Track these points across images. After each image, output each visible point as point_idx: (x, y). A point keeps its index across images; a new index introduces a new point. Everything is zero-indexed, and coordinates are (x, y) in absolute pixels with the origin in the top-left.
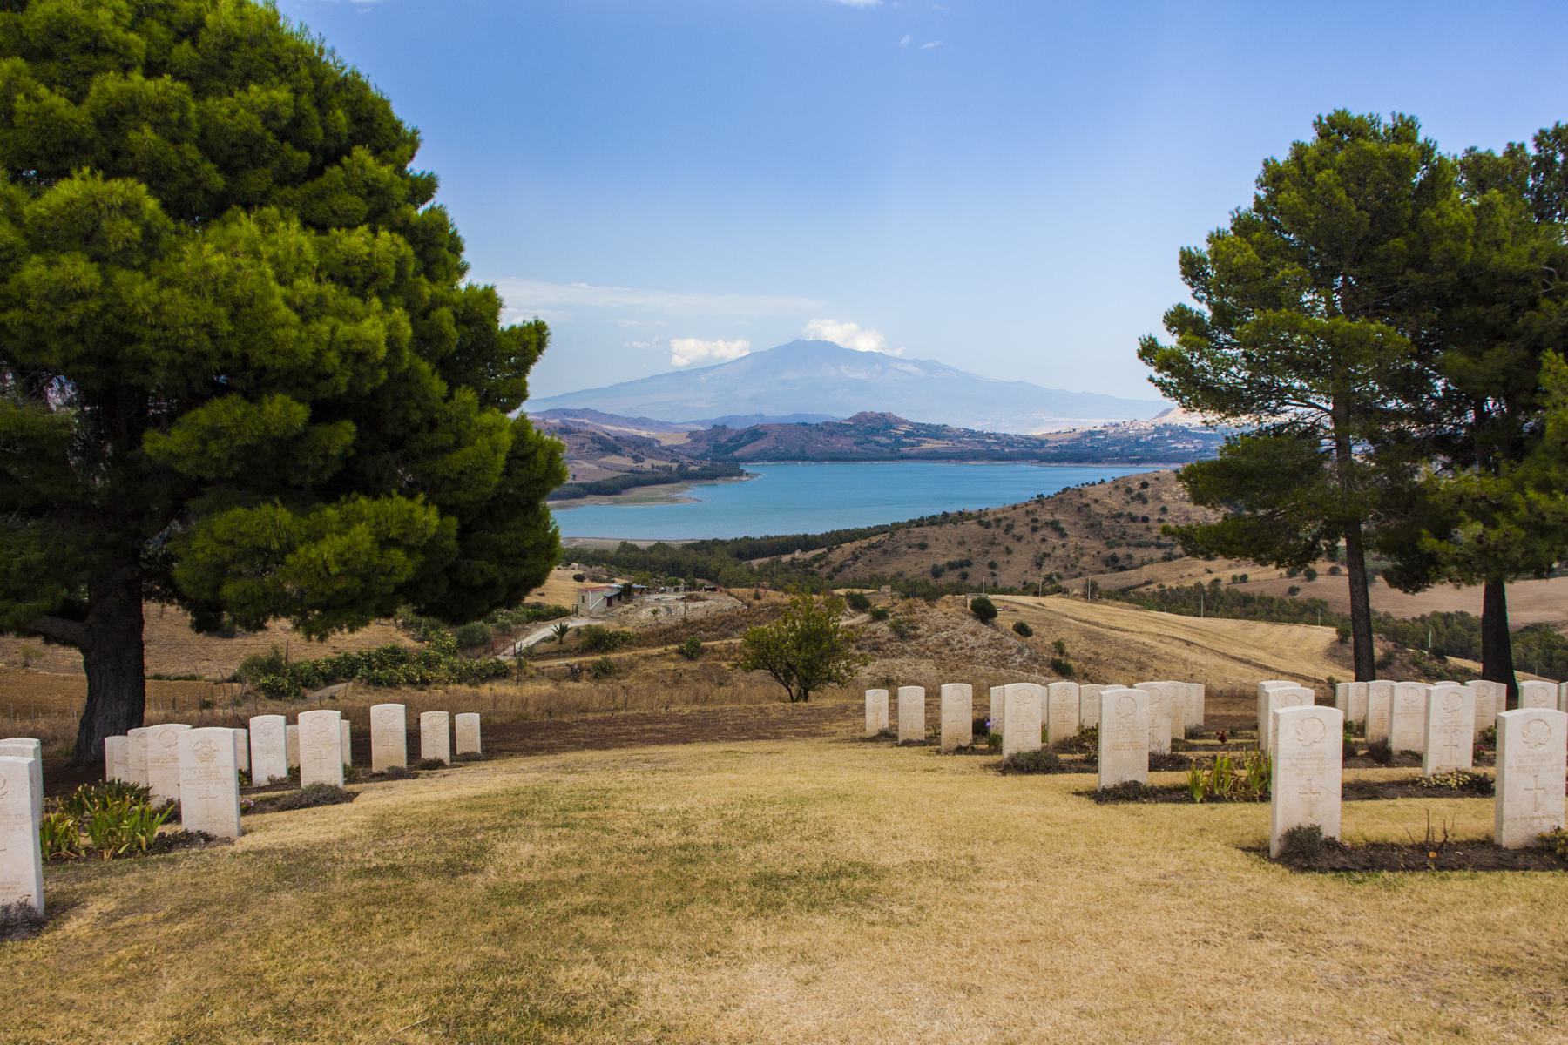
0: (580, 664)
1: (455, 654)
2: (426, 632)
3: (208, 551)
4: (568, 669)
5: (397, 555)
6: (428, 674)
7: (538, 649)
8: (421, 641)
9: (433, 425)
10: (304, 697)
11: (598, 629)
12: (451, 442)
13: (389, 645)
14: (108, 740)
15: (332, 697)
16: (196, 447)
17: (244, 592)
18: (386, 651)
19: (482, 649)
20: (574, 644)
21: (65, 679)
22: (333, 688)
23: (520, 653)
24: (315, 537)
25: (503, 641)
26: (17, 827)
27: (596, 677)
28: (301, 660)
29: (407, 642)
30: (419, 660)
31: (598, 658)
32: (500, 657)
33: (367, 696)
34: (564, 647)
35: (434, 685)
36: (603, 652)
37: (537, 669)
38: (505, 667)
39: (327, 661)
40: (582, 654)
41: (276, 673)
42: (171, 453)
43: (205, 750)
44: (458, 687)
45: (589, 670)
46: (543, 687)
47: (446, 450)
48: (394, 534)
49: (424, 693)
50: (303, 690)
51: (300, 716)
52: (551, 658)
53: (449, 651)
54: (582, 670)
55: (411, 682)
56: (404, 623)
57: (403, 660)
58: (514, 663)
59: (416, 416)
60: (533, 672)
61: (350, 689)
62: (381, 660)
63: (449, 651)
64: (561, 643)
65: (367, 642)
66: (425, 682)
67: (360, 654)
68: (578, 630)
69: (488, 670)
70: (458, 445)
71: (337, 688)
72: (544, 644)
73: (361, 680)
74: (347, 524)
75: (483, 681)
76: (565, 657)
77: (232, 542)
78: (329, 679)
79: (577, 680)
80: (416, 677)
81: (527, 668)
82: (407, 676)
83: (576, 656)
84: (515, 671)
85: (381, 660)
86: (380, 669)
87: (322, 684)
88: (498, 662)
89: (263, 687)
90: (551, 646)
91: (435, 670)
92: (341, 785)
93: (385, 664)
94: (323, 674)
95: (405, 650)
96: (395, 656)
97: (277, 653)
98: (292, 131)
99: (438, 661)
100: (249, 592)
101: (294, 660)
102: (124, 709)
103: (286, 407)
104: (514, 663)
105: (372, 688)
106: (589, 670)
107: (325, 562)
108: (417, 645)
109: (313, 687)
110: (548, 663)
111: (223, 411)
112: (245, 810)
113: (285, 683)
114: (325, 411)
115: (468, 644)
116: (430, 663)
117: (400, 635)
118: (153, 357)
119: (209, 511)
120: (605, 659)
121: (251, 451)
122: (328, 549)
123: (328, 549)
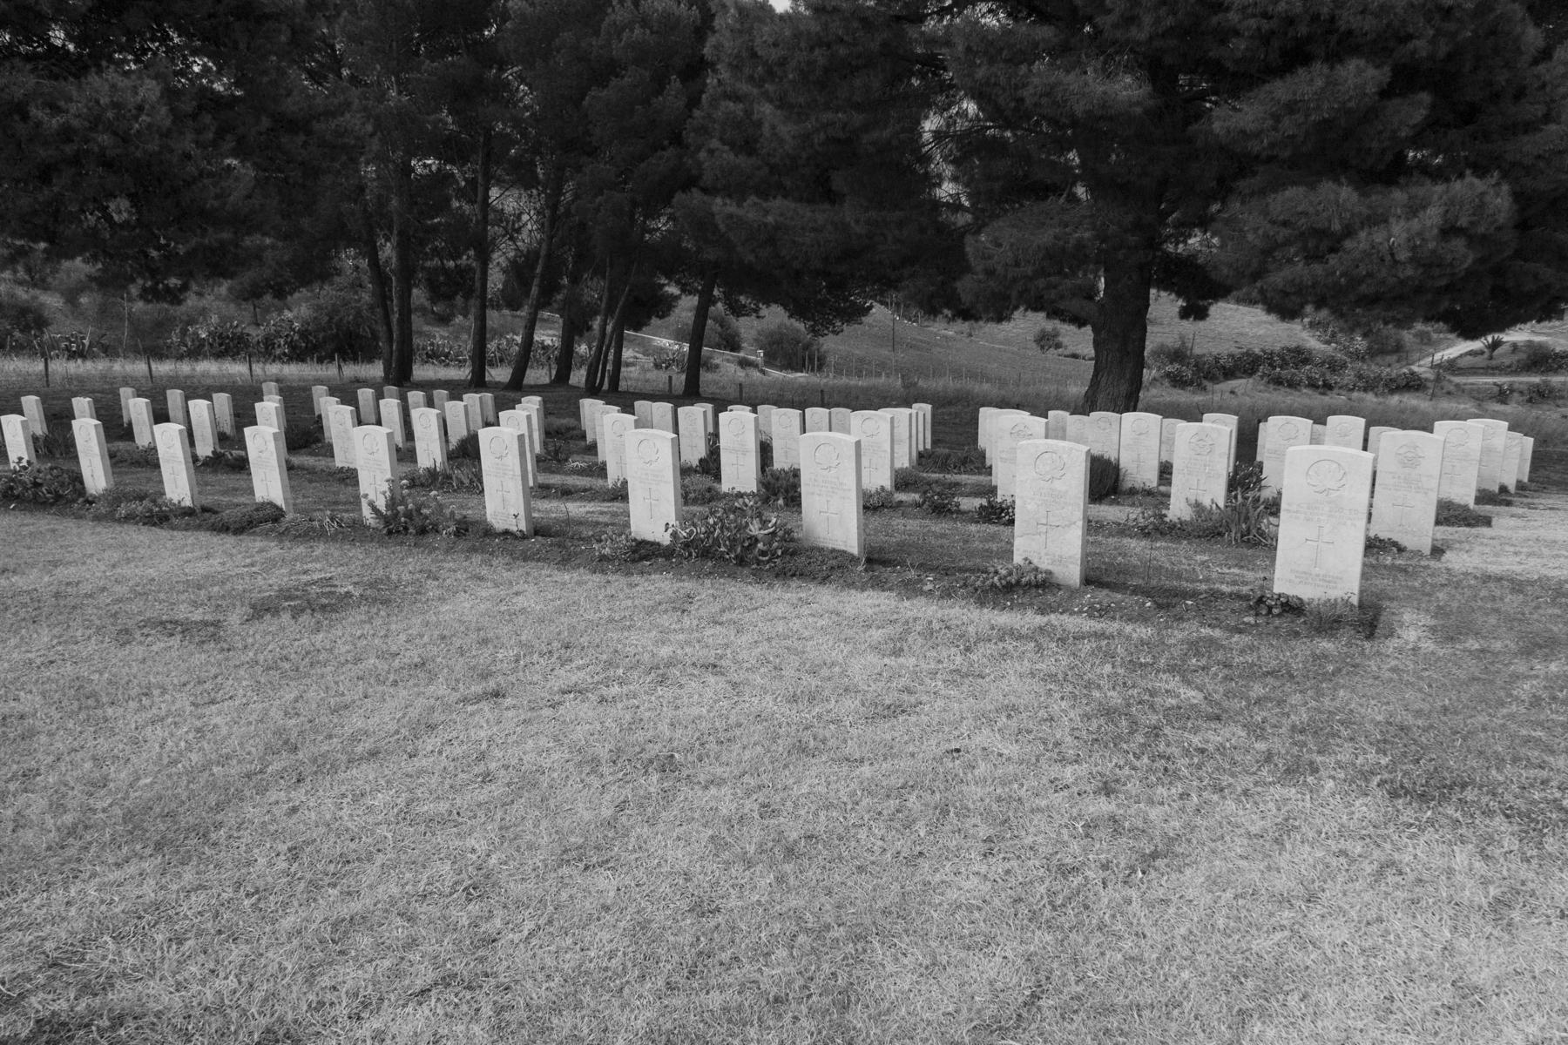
0: (1511, 384)
1: (1363, 359)
2: (1333, 335)
3: (1260, 232)
4: (1496, 389)
5: (1459, 244)
6: (1332, 379)
7: (1463, 363)
8: (1328, 343)
9: (1520, 94)
10: (1204, 389)
11: (1540, 345)
12: (1540, 114)
13: (1294, 345)
14: (982, 410)
15: (1232, 392)
16: (1270, 122)
17: (1293, 281)
18: (1289, 350)
19: (1395, 357)
20: (1507, 362)
21: (1000, 350)
22: (1233, 383)
23: (1439, 366)
24: (1377, 219)
25: (1420, 350)
26: (1349, 522)
27: (1530, 400)
28: (1205, 351)
29: (1312, 342)
30: (1323, 363)
31: (1536, 379)
32: (1415, 368)
33: (1267, 395)
34: (1494, 363)
35: (1336, 391)
36: (1543, 373)
37: (1457, 385)
38: (1419, 379)
39: (1229, 355)
40: (1516, 372)
41: (1182, 363)
42: (1243, 132)
43: (1409, 455)
44: (1362, 395)
45: (1521, 393)
46: (1462, 406)
47: (1529, 127)
48: (1463, 222)
49: (1326, 399)
50: (1205, 383)
51: (1437, 424)
52: (1475, 374)
53: (1358, 356)
54: (1512, 391)
55: (1313, 385)
56: (1311, 323)
57: (1306, 361)
58: (1430, 375)
59: (1502, 78)
60: (1452, 388)
61: (1250, 386)
62: (1283, 359)
63: (1358, 356)
64: (1491, 358)
65: (1269, 340)
66: (1328, 387)
67: (1263, 351)
68: (1515, 347)
69: (1399, 381)
70: (1547, 118)
71: (1239, 384)
72: (1469, 357)
73: (1262, 377)
74: (1414, 210)
75: (1392, 392)
76: (1493, 375)
77: (1285, 224)
78: (1229, 373)
79: (1504, 402)
80: (1318, 380)
81: (1445, 383)
82: (1309, 378)
83: (1507, 374)
84: (1430, 385)
85: (1283, 359)
86: (1281, 367)
87: (1221, 378)
88: (1413, 373)
89: (1168, 375)
90: (1480, 361)
91: (1340, 375)
92: (1472, 505)
93: (1287, 364)
94: (1224, 367)
95: (1310, 352)
96: (1300, 356)
97: (1183, 343)
99: (1344, 366)
100: (1297, 281)
101: (1197, 351)
102: (1124, 388)
103: (1360, 71)
104: (1430, 375)
105: (1272, 386)
106: (1521, 393)
107: (1391, 248)
108: (1323, 346)
109: (1213, 379)
110: (1472, 380)
111: (1307, 83)
112: (379, 423)
113: (1188, 373)
114: (1405, 80)
115: (1380, 349)
116: (1334, 366)
117: (1305, 335)
118: (1238, 27)
119: (1263, 192)
120: (1544, 382)
121: (1326, 125)
122: (1398, 233)
123: (1398, 233)
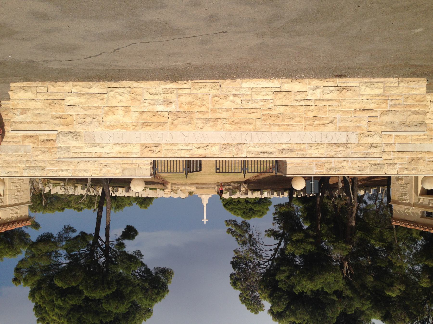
98: (229, 205)
